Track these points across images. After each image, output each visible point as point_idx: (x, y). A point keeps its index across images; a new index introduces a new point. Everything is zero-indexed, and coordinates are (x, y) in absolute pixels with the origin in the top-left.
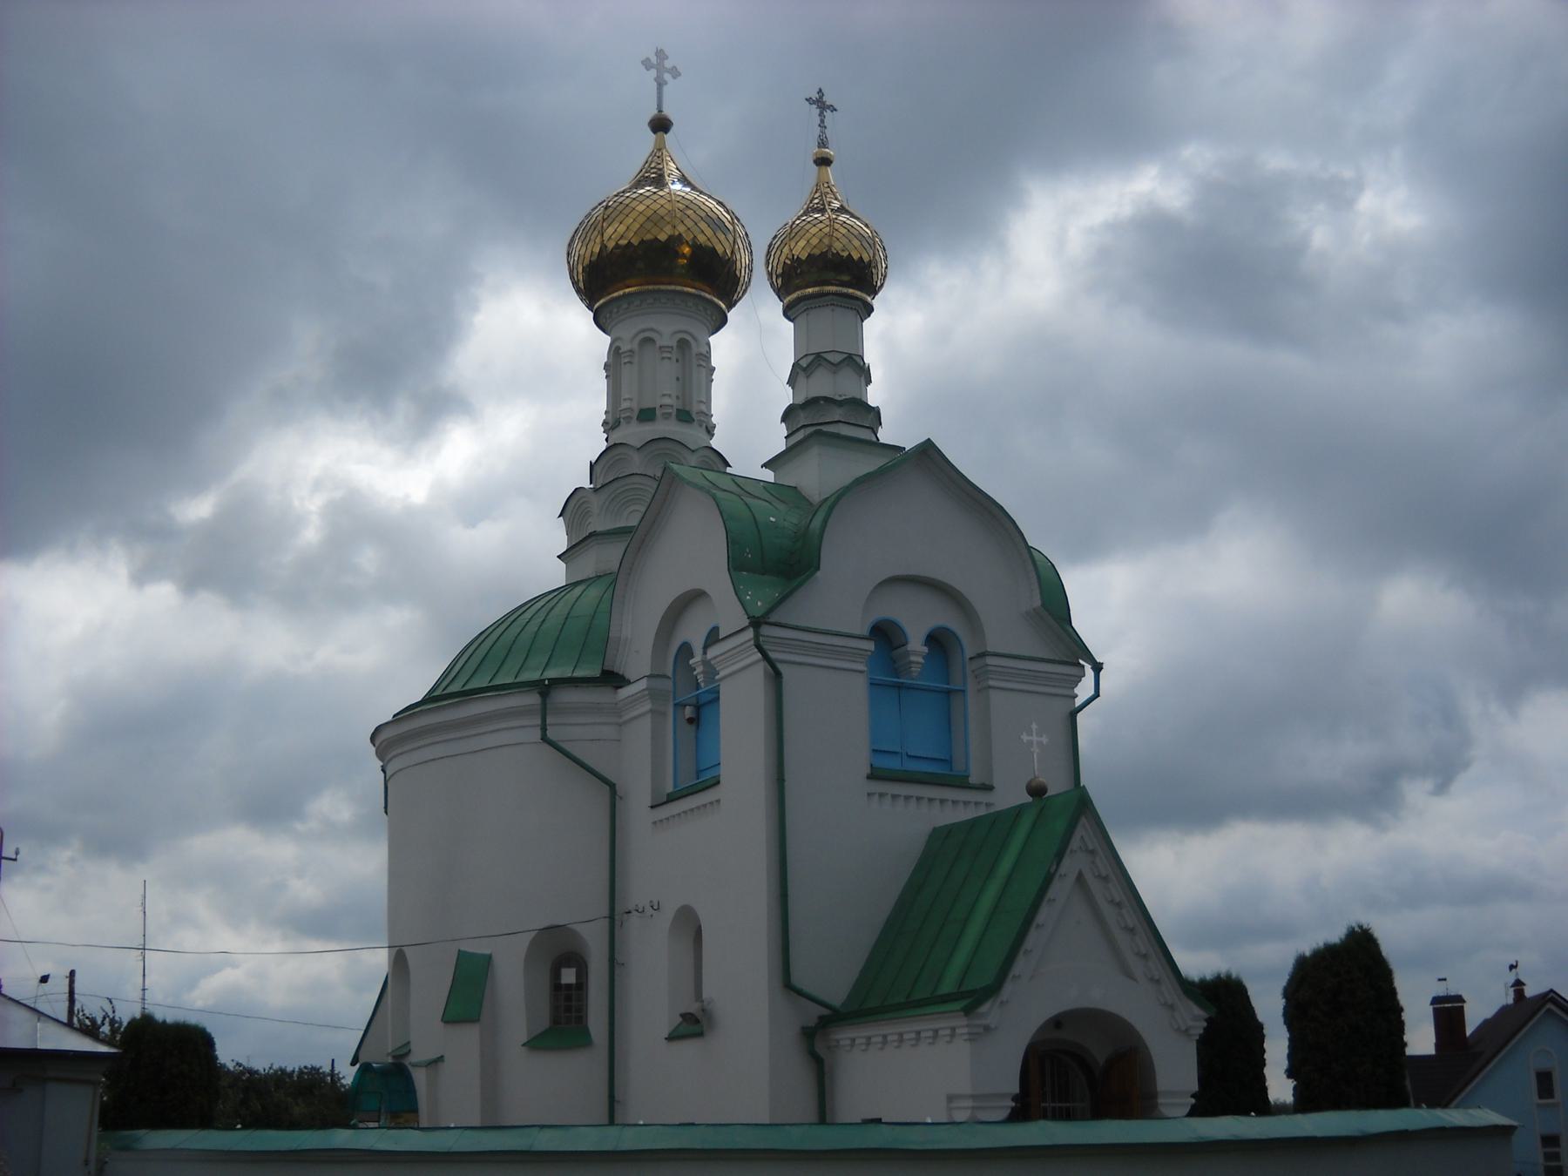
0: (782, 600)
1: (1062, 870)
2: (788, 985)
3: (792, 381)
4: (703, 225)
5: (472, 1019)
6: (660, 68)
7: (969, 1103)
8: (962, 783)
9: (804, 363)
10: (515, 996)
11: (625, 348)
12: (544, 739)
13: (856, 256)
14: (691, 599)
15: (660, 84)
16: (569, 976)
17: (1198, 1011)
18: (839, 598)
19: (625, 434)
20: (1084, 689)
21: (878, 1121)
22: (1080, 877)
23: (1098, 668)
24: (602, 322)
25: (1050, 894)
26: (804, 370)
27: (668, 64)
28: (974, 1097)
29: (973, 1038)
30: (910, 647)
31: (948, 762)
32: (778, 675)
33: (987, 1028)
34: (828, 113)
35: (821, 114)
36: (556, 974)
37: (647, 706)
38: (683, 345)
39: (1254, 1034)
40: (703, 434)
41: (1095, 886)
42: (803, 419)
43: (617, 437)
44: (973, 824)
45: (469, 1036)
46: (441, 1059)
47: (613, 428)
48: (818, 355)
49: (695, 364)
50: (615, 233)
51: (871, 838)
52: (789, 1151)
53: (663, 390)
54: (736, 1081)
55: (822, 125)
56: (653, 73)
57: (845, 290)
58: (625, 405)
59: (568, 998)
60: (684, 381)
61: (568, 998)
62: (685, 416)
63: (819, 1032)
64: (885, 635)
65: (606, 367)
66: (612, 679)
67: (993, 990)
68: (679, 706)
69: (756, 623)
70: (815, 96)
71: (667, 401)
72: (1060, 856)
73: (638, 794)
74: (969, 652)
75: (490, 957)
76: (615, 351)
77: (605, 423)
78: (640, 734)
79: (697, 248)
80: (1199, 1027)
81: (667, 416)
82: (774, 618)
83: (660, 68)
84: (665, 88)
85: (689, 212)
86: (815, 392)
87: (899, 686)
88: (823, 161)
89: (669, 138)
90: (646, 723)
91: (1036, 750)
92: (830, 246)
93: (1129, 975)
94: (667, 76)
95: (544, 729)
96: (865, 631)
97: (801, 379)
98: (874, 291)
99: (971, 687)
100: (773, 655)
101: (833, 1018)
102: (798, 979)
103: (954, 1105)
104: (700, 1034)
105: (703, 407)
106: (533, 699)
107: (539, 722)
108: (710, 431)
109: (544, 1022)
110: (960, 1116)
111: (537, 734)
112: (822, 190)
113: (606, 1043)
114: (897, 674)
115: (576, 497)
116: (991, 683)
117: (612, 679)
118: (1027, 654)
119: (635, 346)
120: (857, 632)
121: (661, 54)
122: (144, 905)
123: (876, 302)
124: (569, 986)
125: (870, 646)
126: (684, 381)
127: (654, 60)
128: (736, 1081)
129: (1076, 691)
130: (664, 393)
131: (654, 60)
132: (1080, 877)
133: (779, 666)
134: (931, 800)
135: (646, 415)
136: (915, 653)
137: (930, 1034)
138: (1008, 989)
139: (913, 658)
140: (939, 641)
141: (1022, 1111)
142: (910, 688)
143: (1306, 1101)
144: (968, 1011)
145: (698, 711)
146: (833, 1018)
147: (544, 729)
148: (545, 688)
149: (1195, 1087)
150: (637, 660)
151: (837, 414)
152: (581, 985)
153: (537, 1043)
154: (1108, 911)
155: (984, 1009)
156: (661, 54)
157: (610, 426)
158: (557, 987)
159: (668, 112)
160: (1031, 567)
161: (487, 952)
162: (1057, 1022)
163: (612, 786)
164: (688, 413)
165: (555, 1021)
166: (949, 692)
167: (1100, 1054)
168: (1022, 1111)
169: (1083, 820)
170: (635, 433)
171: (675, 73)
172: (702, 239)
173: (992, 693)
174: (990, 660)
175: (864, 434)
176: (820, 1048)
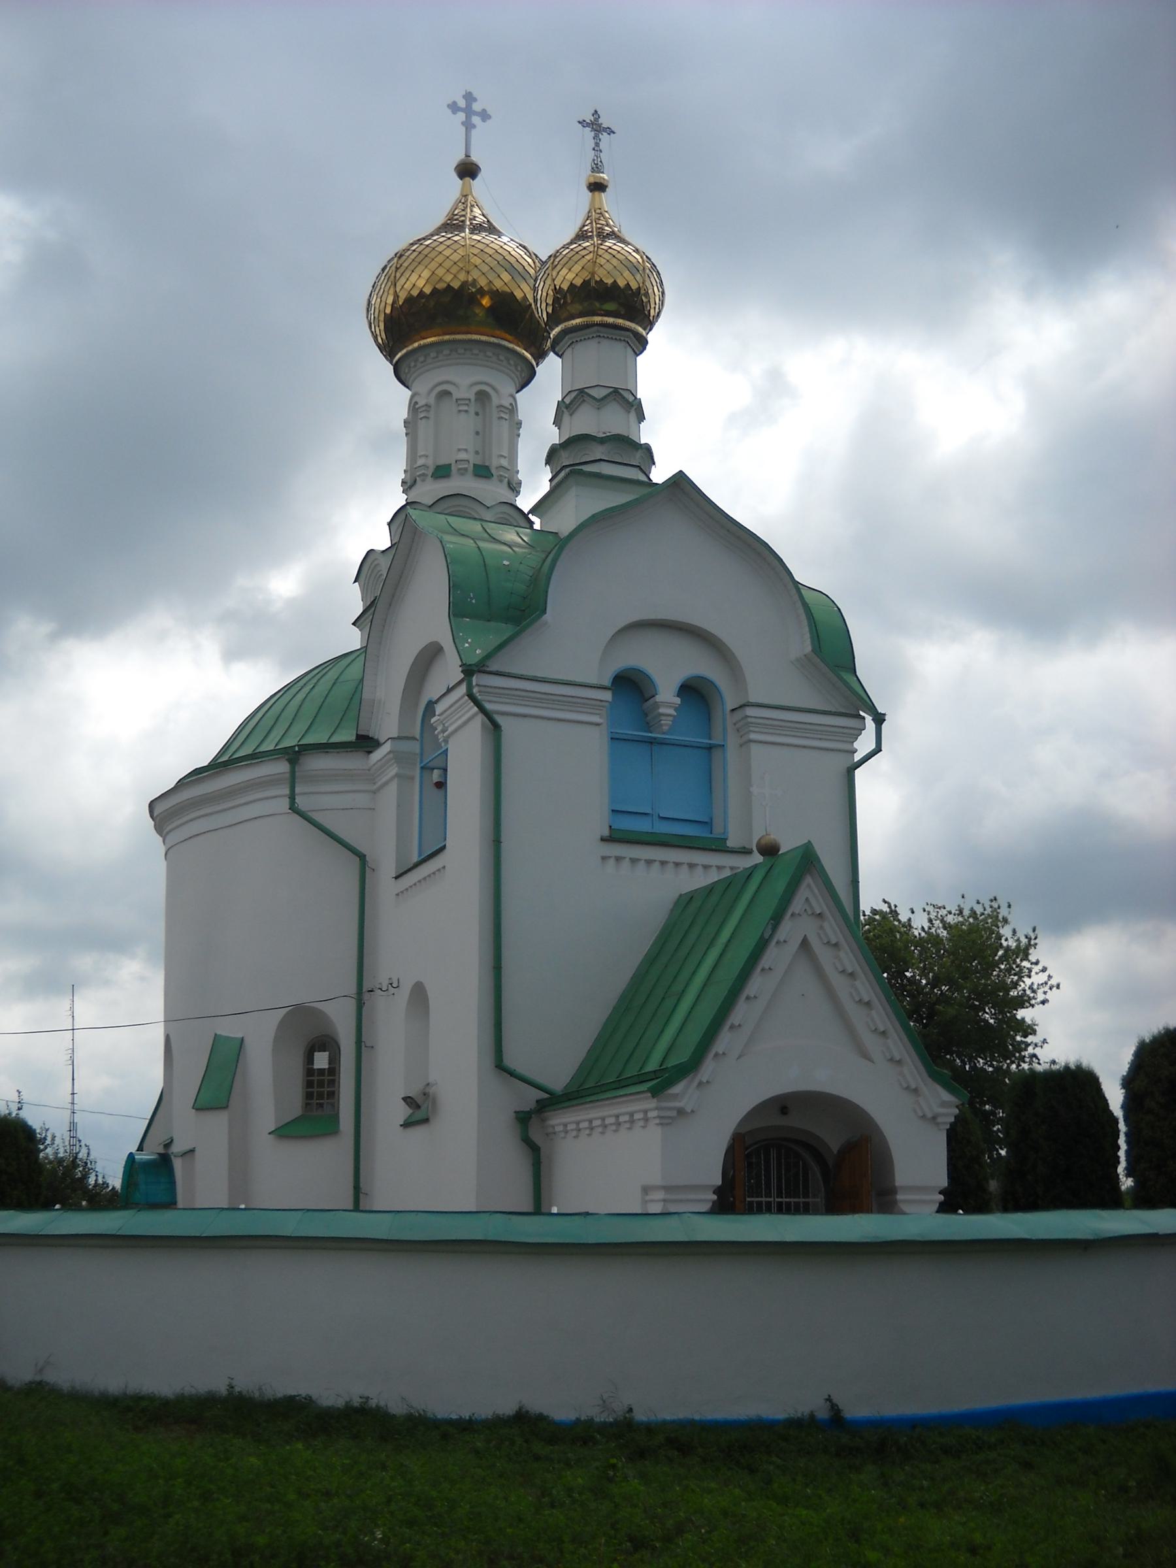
0: (501, 647)
1: (781, 934)
2: (500, 1066)
3: (557, 422)
4: (499, 270)
5: (221, 1105)
6: (469, 112)
7: (660, 1195)
8: (718, 846)
9: (567, 401)
10: (267, 1085)
12: (293, 808)
13: (622, 283)
14: (430, 655)
15: (468, 126)
16: (321, 1061)
17: (946, 1096)
18: (575, 641)
19: (418, 494)
20: (864, 743)
21: (587, 1214)
22: (805, 943)
23: (879, 719)
24: (403, 377)
25: (766, 961)
26: (567, 407)
27: (476, 107)
30: (658, 698)
31: (708, 824)
32: (496, 726)
33: (681, 1112)
34: (604, 137)
36: (310, 1059)
37: (393, 770)
38: (482, 397)
39: (1116, 1121)
40: (504, 494)
41: (824, 955)
42: (565, 459)
43: (415, 495)
44: (710, 889)
45: (219, 1122)
46: (192, 1151)
47: (410, 487)
48: (581, 391)
50: (418, 281)
51: (602, 906)
52: (574, 1244)
54: (444, 1169)
55: (597, 148)
56: (461, 116)
57: (610, 320)
58: (420, 462)
62: (483, 472)
63: (535, 1118)
64: (631, 686)
65: (405, 422)
66: (366, 743)
69: (469, 671)
70: (589, 118)
71: (463, 456)
72: (776, 919)
73: (386, 865)
74: (730, 703)
75: (242, 1039)
76: (413, 407)
77: (404, 483)
79: (496, 295)
80: (949, 1114)
81: (463, 472)
83: (469, 112)
84: (474, 132)
87: (651, 742)
88: (597, 187)
89: (477, 185)
90: (393, 788)
92: (593, 274)
93: (866, 1056)
94: (476, 120)
95: (292, 797)
96: (607, 682)
97: (566, 418)
98: (649, 324)
99: (732, 742)
101: (551, 1102)
102: (510, 1061)
103: (648, 1198)
104: (426, 1121)
105: (504, 462)
107: (287, 791)
109: (295, 1107)
110: (656, 1208)
111: (285, 803)
112: (596, 214)
113: (352, 1131)
114: (648, 727)
115: (369, 560)
116: (753, 736)
118: (766, 701)
119: (432, 400)
120: (594, 681)
121: (469, 97)
123: (651, 337)
124: (321, 1071)
125: (607, 696)
127: (462, 103)
128: (444, 1169)
129: (856, 745)
131: (462, 103)
132: (805, 943)
133: (499, 719)
134: (677, 864)
135: (442, 472)
136: (668, 705)
137: (627, 1118)
138: (708, 1068)
139: (662, 710)
140: (695, 692)
141: (727, 1201)
142: (662, 743)
143: (1144, 1199)
144: (655, 1092)
146: (551, 1102)
147: (292, 797)
148: (294, 755)
149: (944, 1182)
150: (387, 725)
151: (598, 452)
152: (333, 1070)
153: (284, 1132)
154: (839, 982)
155: (677, 1089)
156: (469, 97)
157: (408, 486)
158: (310, 1071)
159: (474, 158)
161: (240, 1035)
162: (782, 1104)
163: (362, 857)
164: (487, 468)
165: (307, 1106)
166: (710, 748)
167: (834, 1142)
168: (727, 1201)
169: (808, 880)
170: (430, 491)
171: (485, 116)
172: (498, 284)
173: (753, 746)
174: (750, 711)
175: (643, 478)
176: (536, 1136)
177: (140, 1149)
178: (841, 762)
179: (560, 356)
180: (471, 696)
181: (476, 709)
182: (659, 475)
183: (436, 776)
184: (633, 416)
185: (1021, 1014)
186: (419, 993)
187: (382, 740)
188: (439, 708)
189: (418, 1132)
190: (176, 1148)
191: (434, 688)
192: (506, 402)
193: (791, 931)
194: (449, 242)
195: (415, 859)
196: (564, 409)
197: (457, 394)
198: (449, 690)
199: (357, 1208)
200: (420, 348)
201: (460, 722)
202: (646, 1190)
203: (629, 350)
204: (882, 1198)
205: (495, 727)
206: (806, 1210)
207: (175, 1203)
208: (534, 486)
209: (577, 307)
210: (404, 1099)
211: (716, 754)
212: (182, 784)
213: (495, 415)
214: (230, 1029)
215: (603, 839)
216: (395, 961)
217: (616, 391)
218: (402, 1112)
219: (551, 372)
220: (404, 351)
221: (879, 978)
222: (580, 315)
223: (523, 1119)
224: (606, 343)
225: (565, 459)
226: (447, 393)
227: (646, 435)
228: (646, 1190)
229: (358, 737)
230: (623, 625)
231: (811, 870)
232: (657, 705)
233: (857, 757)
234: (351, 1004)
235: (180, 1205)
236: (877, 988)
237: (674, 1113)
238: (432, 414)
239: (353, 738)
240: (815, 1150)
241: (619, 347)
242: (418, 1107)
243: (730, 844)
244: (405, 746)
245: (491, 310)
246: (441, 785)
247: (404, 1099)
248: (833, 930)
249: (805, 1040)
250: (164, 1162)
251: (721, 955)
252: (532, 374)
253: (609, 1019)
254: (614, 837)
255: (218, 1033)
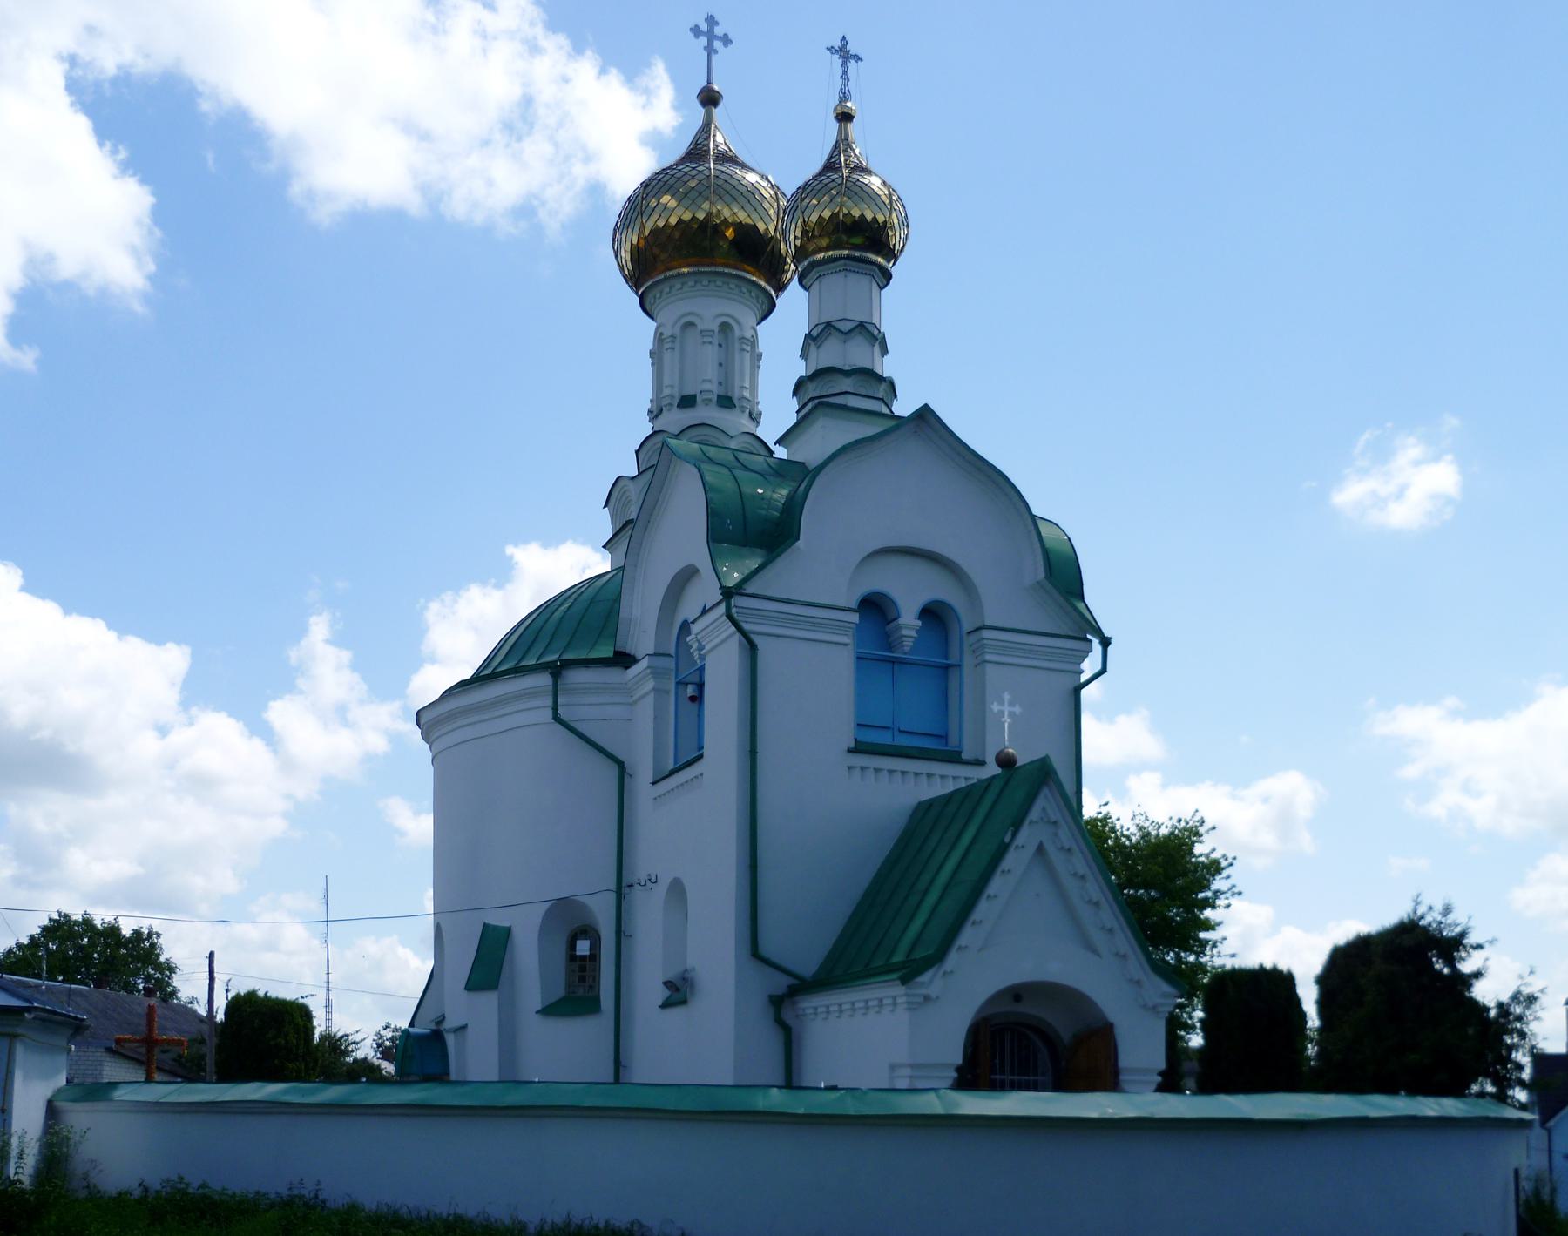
2: (755, 953)
3: (804, 354)
6: (711, 36)
7: (908, 1071)
8: (954, 757)
9: (814, 333)
10: (532, 969)
11: (667, 332)
12: (556, 718)
14: (687, 576)
15: (710, 51)
16: (583, 947)
18: (824, 566)
20: (1090, 666)
22: (1040, 849)
23: (1106, 643)
26: (815, 339)
27: (718, 31)
28: (912, 1066)
29: (912, 1007)
30: (901, 621)
31: (944, 737)
32: (753, 647)
33: (927, 998)
35: (844, 64)
36: (572, 946)
37: (650, 684)
38: (725, 328)
40: (747, 425)
42: (812, 390)
43: (661, 423)
44: (949, 797)
45: (489, 1000)
46: (464, 1027)
48: (828, 324)
49: (734, 346)
51: (845, 805)
53: (705, 375)
54: (699, 1043)
56: (703, 41)
58: (667, 392)
59: (583, 969)
60: (724, 365)
61: (583, 969)
62: (726, 402)
63: (787, 997)
64: (875, 608)
65: (651, 353)
66: (624, 660)
67: (938, 957)
68: (681, 684)
69: (728, 594)
71: (707, 386)
72: (1017, 826)
73: (643, 771)
76: (659, 338)
77: (650, 412)
78: (645, 713)
79: (740, 227)
81: (707, 402)
82: (751, 588)
83: (711, 36)
84: (716, 58)
85: (728, 187)
86: (826, 362)
87: (894, 661)
89: (716, 112)
90: (650, 699)
91: (1007, 721)
94: (717, 44)
96: (854, 604)
98: (892, 255)
99: (968, 661)
100: (746, 627)
101: (802, 987)
102: (768, 947)
104: (684, 1002)
106: (545, 679)
107: (550, 702)
108: (755, 418)
109: (560, 992)
113: (217, 986)
114: (890, 648)
116: (988, 657)
117: (624, 660)
118: (1000, 625)
120: (842, 603)
121: (711, 21)
122: (326, 897)
123: (896, 270)
124: (583, 958)
125: (855, 618)
126: (724, 365)
127: (704, 27)
128: (699, 1043)
130: (705, 378)
131: (704, 27)
132: (1040, 849)
133: (756, 639)
134: (891, 772)
135: (687, 402)
136: (908, 626)
137: (889, 1001)
139: (904, 632)
140: (934, 614)
141: (970, 1077)
144: (905, 981)
145: (694, 692)
151: (846, 384)
152: (594, 957)
153: (548, 1011)
154: (1071, 885)
156: (711, 21)
157: (654, 414)
158: (572, 957)
159: (887, 166)
160: (1036, 539)
162: (1016, 993)
163: (621, 764)
166: (947, 668)
167: (1065, 1029)
168: (975, 1072)
169: (1045, 791)
170: (676, 419)
174: (986, 634)
175: (885, 410)
176: (788, 1016)
177: (412, 1025)
178: (1068, 683)
179: (807, 289)
180: (729, 617)
181: (733, 628)
182: (903, 407)
183: (690, 691)
184: (877, 349)
185: (1208, 913)
186: (677, 889)
187: (639, 656)
188: (695, 628)
189: (676, 1013)
190: (447, 1025)
191: (689, 609)
192: (748, 334)
193: (1028, 836)
194: (693, 173)
195: (671, 766)
196: (812, 340)
197: (700, 327)
198: (705, 612)
199: (617, 1081)
200: (666, 279)
201: (717, 641)
202: (893, 1067)
203: (875, 285)
204: (1105, 1077)
205: (751, 647)
206: (1035, 1087)
207: (448, 1074)
208: (776, 411)
209: (824, 242)
210: (665, 983)
211: (954, 676)
212: (448, 694)
213: (737, 346)
214: (498, 919)
215: (849, 751)
216: (649, 859)
217: (861, 325)
218: (661, 994)
219: (794, 308)
220: (762, 283)
221: (1108, 881)
222: (827, 249)
223: (778, 1003)
224: (853, 277)
225: (812, 390)
226: (691, 324)
227: (888, 367)
228: (893, 1067)
229: (616, 653)
230: (871, 550)
231: (1049, 779)
232: (899, 628)
233: (1084, 678)
234: (612, 897)
235: (453, 1077)
236: (1105, 888)
237: (921, 1000)
238: (677, 346)
239: (611, 654)
240: (1047, 1036)
241: (865, 280)
242: (678, 990)
243: (965, 756)
244: (661, 662)
245: (734, 243)
246: (697, 699)
247: (665, 983)
248: (1066, 836)
249: (1024, 937)
250: (436, 1039)
251: (964, 858)
252: (772, 306)
253: (854, 914)
254: (859, 748)
255: (492, 921)
